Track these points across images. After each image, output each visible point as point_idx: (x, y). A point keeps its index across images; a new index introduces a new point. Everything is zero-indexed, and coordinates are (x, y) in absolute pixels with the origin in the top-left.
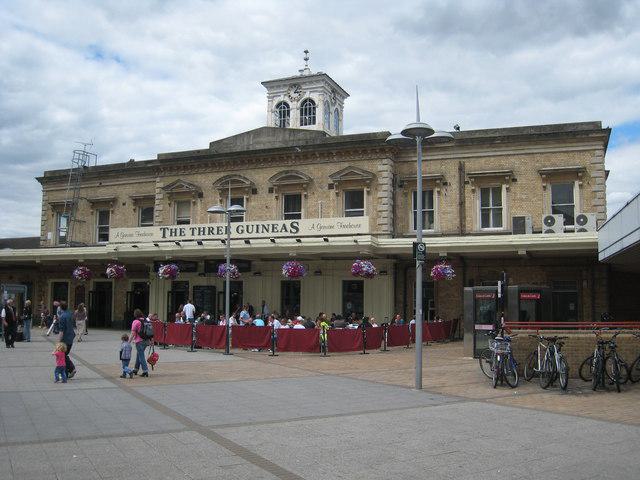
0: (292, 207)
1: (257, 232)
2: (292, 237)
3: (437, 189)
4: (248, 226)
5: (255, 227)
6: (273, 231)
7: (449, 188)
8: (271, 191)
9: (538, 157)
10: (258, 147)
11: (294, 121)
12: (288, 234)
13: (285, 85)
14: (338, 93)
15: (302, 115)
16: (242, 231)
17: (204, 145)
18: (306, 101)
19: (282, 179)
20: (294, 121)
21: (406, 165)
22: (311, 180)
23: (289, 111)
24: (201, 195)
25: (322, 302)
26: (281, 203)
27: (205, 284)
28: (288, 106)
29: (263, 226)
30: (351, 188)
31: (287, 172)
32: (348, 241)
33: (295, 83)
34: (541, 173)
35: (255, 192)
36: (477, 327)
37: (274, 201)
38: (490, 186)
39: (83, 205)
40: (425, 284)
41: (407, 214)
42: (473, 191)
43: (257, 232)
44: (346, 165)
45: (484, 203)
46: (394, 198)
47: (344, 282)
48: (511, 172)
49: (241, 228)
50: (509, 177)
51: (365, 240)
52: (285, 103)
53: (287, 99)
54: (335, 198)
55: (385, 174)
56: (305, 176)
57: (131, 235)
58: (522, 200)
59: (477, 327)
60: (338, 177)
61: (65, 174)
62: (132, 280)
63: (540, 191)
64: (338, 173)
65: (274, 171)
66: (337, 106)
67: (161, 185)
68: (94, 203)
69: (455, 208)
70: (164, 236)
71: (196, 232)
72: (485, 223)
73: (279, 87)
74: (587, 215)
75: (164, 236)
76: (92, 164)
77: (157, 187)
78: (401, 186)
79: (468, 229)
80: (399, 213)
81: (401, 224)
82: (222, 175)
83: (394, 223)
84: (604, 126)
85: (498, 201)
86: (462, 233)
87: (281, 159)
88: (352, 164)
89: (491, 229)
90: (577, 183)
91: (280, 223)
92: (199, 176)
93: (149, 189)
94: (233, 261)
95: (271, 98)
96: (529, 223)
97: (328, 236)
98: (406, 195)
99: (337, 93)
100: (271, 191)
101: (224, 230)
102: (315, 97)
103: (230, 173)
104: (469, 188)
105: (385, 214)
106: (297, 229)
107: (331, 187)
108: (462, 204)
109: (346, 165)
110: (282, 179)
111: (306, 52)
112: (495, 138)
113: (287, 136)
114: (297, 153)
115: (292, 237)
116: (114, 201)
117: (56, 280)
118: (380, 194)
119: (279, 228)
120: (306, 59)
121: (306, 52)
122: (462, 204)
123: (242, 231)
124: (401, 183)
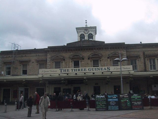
0: (76, 64)
1: (96, 70)
2: (66, 73)
5: (95, 69)
6: (101, 70)
8: (89, 59)
10: (83, 45)
11: (86, 38)
12: (107, 71)
15: (80, 38)
16: (90, 70)
18: (89, 34)
20: (86, 38)
24: (64, 60)
26: (54, 64)
27: (67, 88)
28: (84, 35)
29: (98, 68)
30: (75, 60)
33: (86, 29)
35: (83, 59)
38: (25, 63)
42: (148, 60)
43: (96, 70)
45: (151, 63)
47: (114, 86)
52: (83, 34)
53: (83, 33)
57: (48, 72)
60: (111, 55)
62: (36, 88)
64: (111, 54)
67: (50, 56)
68: (21, 62)
69: (143, 65)
70: (61, 72)
71: (73, 70)
72: (151, 69)
75: (61, 72)
79: (147, 70)
85: (154, 62)
86: (145, 71)
87: (92, 49)
90: (156, 59)
97: (113, 72)
100: (89, 59)
104: (146, 59)
106: (110, 69)
107: (108, 58)
108: (145, 63)
110: (74, 56)
111: (86, 21)
113: (93, 43)
115: (66, 73)
117: (37, 88)
119: (103, 69)
120: (86, 23)
122: (145, 63)
123: (90, 70)
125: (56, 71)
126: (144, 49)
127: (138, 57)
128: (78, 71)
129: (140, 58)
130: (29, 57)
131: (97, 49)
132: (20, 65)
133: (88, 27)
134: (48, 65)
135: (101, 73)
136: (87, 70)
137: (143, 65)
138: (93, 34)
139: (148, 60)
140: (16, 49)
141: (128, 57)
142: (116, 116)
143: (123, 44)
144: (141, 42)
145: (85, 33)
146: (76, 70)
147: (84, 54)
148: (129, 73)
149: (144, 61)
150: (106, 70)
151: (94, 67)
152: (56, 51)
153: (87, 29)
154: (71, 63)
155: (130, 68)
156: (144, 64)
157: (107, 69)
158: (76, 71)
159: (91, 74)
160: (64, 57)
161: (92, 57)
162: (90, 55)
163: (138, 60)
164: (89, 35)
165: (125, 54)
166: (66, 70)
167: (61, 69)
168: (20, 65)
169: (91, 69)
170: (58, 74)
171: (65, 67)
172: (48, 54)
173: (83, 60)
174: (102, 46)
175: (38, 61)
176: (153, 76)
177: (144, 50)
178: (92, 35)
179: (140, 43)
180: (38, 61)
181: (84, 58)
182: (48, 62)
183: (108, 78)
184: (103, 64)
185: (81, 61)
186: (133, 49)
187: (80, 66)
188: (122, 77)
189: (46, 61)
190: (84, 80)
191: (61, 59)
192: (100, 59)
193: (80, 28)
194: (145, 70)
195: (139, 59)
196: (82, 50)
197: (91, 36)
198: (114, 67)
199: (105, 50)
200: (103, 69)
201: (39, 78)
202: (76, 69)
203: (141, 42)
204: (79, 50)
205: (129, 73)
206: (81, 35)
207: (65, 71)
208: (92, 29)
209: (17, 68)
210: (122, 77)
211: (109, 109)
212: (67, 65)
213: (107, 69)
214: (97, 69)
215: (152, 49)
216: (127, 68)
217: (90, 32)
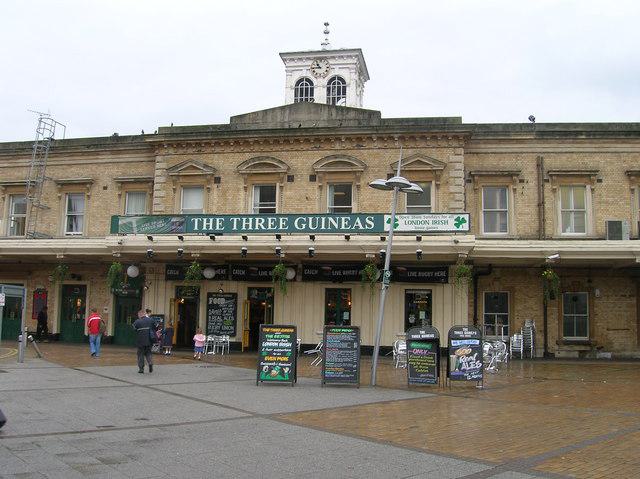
7: (525, 185)
8: (313, 178)
11: (320, 96)
13: (309, 59)
15: (328, 94)
17: (223, 119)
18: (333, 79)
19: (255, 166)
24: (218, 180)
25: (100, 309)
28: (312, 83)
30: (261, 181)
31: (335, 157)
33: (320, 57)
35: (291, 179)
37: (317, 192)
39: (49, 188)
40: (72, 286)
50: (86, 184)
52: (308, 80)
55: (458, 166)
56: (361, 163)
58: (607, 202)
63: (627, 194)
65: (317, 155)
67: (164, 165)
69: (533, 209)
76: (58, 136)
79: (548, 231)
82: (248, 156)
86: (541, 235)
89: (497, 234)
94: (553, 268)
96: (626, 228)
99: (363, 73)
100: (313, 178)
102: (345, 74)
103: (258, 154)
104: (548, 186)
108: (541, 204)
110: (255, 166)
111: (326, 24)
112: (580, 133)
116: (91, 183)
118: (453, 189)
122: (541, 204)
126: (540, 147)
129: (522, 181)
132: (60, 198)
134: (155, 201)
136: (305, 222)
138: (347, 81)
139: (554, 191)
140: (47, 135)
141: (473, 176)
142: (145, 386)
144: (532, 118)
145: (317, 76)
148: (454, 245)
149: (536, 195)
152: (189, 145)
153: (325, 58)
154: (242, 193)
156: (539, 205)
160: (215, 170)
163: (515, 190)
164: (329, 83)
165: (460, 166)
168: (60, 198)
172: (158, 158)
173: (215, 186)
174: (374, 128)
177: (539, 150)
178: (344, 82)
180: (63, 184)
182: (156, 186)
185: (281, 187)
186: (71, 155)
187: (433, 205)
188: (392, 255)
189: (150, 181)
190: (277, 262)
191: (435, 171)
192: (358, 179)
193: (298, 53)
194: (539, 231)
195: (519, 187)
198: (410, 218)
201: (110, 249)
203: (532, 118)
205: (454, 245)
206: (298, 83)
210: (392, 255)
212: (226, 200)
215: (574, 148)
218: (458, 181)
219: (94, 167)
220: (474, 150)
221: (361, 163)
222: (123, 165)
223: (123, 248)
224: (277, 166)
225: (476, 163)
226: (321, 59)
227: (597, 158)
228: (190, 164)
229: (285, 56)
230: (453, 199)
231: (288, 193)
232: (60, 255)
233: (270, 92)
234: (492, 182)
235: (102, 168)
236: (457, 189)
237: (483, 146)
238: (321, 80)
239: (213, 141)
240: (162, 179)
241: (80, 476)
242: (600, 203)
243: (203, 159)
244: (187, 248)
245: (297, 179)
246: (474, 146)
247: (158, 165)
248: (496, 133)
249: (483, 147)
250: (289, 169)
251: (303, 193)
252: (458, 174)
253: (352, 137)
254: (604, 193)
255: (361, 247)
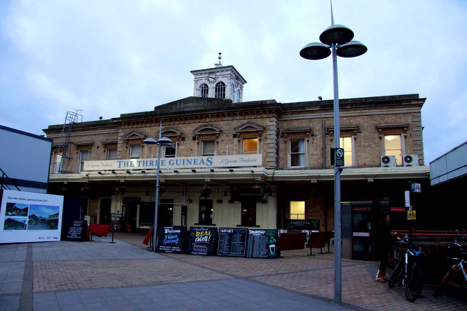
1: (183, 164)
3: (307, 139)
4: (177, 160)
5: (182, 161)
6: (194, 164)
7: (315, 138)
8: (194, 139)
9: (376, 118)
10: (186, 110)
11: (211, 94)
13: (205, 73)
14: (240, 80)
15: (216, 92)
16: (173, 164)
18: (219, 83)
20: (211, 94)
21: (286, 123)
22: (221, 131)
23: (208, 90)
28: (207, 86)
29: (188, 160)
31: (205, 126)
32: (247, 171)
34: (377, 128)
36: (355, 234)
41: (286, 155)
43: (183, 164)
44: (246, 121)
46: (277, 144)
48: (358, 127)
49: (172, 162)
51: (260, 170)
54: (237, 143)
55: (272, 128)
56: (218, 128)
58: (364, 146)
59: (355, 234)
60: (240, 130)
61: (61, 127)
64: (241, 126)
65: (196, 125)
66: (239, 88)
67: (122, 134)
73: (201, 74)
74: (412, 156)
75: (139, 165)
77: (121, 134)
78: (282, 137)
80: (281, 154)
81: (282, 162)
83: (277, 162)
84: (420, 97)
87: (202, 117)
88: (249, 120)
91: (200, 158)
92: (147, 128)
93: (114, 137)
95: (196, 81)
98: (286, 142)
99: (239, 80)
100: (194, 139)
101: (154, 164)
102: (225, 80)
105: (272, 155)
107: (235, 136)
109: (246, 121)
110: (202, 130)
111: (220, 54)
114: (212, 110)
116: (92, 145)
118: (268, 141)
119: (199, 162)
120: (220, 58)
121: (220, 54)
123: (173, 164)
124: (281, 134)
125: (112, 165)
127: (307, 133)
128: (150, 165)
129: (313, 135)
130: (91, 136)
131: (212, 116)
132: (77, 153)
133: (223, 66)
135: (191, 170)
137: (319, 153)
138: (226, 84)
143: (273, 103)
144: (320, 98)
146: (145, 162)
147: (185, 129)
149: (321, 144)
150: (204, 164)
151: (204, 155)
152: (134, 124)
155: (255, 161)
156: (323, 149)
157: (205, 161)
158: (127, 166)
159: (189, 172)
161: (199, 135)
162: (195, 130)
163: (308, 141)
164: (216, 86)
166: (147, 161)
167: (120, 162)
169: (175, 161)
170: (209, 170)
171: (148, 157)
172: (120, 131)
173: (182, 142)
175: (106, 145)
176: (374, 180)
179: (319, 100)
181: (184, 138)
182: (119, 146)
183: (207, 182)
184: (221, 151)
185: (178, 144)
187: (176, 155)
192: (217, 138)
195: (311, 139)
196: (181, 119)
197: (222, 88)
199: (241, 118)
200: (199, 162)
202: (147, 161)
204: (176, 120)
207: (145, 165)
208: (222, 71)
209: (72, 159)
211: (69, 233)
212: (151, 151)
213: (205, 161)
214: (186, 161)
216: (249, 161)
217: (220, 79)
218: (272, 137)
219: (93, 136)
220: (285, 119)
221: (218, 128)
222: (106, 135)
223: (89, 178)
224: (176, 133)
225: (285, 126)
226: (212, 73)
227: (358, 120)
228: (133, 133)
229: (191, 72)
230: (269, 147)
231: (181, 147)
232: (314, 181)
233: (186, 89)
234: (294, 138)
235: (97, 137)
236: (272, 141)
237: (290, 116)
238: (212, 84)
239: (145, 120)
240: (121, 142)
241: (324, 310)
242: (360, 146)
243: (141, 130)
244: (117, 177)
245: (186, 139)
246: (285, 116)
247: (120, 134)
248: (297, 108)
249: (290, 117)
250: (182, 134)
251: (189, 146)
252: (272, 133)
253: (214, 114)
254: (362, 140)
255: (202, 176)
